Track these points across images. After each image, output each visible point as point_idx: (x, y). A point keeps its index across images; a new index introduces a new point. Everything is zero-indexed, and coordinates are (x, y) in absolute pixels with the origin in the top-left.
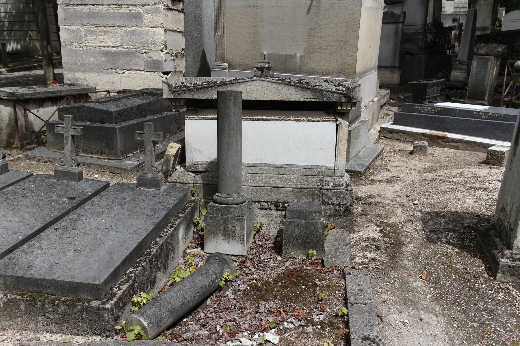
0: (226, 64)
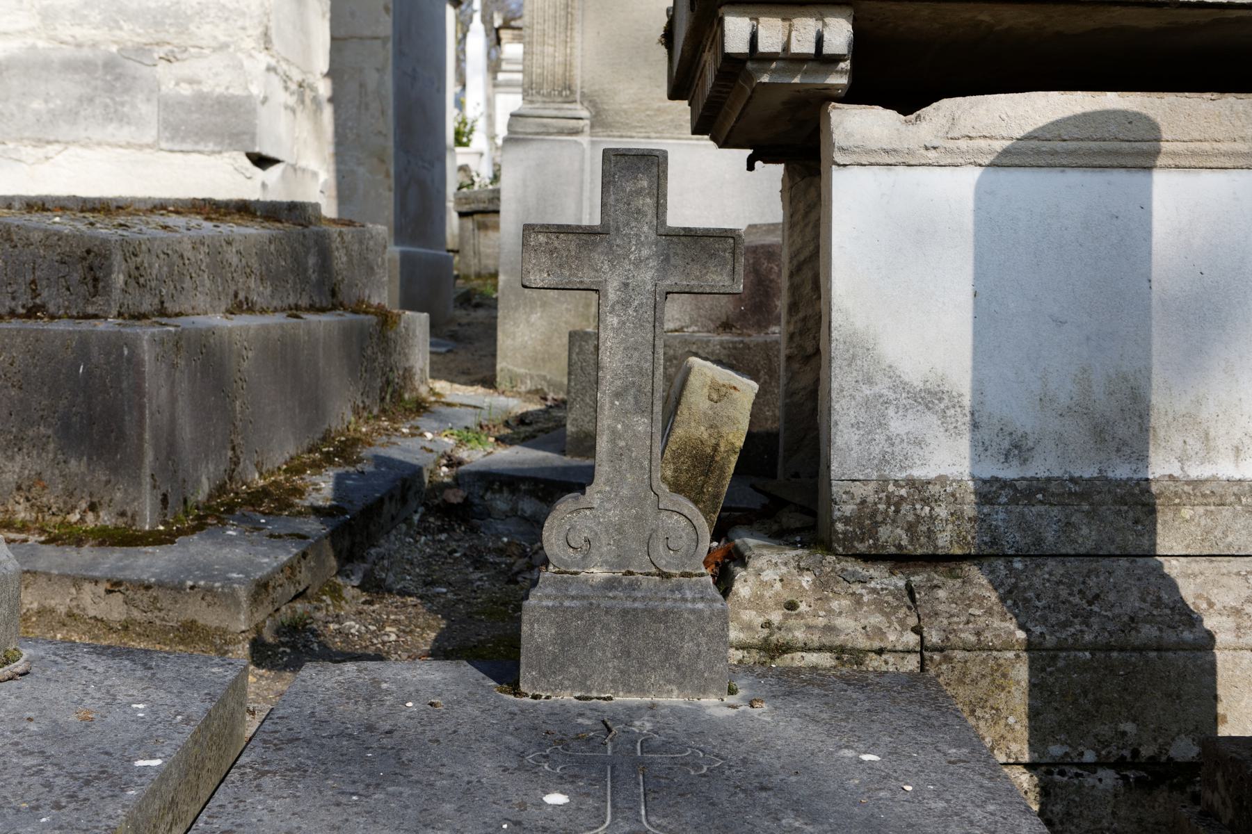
0: (585, 113)
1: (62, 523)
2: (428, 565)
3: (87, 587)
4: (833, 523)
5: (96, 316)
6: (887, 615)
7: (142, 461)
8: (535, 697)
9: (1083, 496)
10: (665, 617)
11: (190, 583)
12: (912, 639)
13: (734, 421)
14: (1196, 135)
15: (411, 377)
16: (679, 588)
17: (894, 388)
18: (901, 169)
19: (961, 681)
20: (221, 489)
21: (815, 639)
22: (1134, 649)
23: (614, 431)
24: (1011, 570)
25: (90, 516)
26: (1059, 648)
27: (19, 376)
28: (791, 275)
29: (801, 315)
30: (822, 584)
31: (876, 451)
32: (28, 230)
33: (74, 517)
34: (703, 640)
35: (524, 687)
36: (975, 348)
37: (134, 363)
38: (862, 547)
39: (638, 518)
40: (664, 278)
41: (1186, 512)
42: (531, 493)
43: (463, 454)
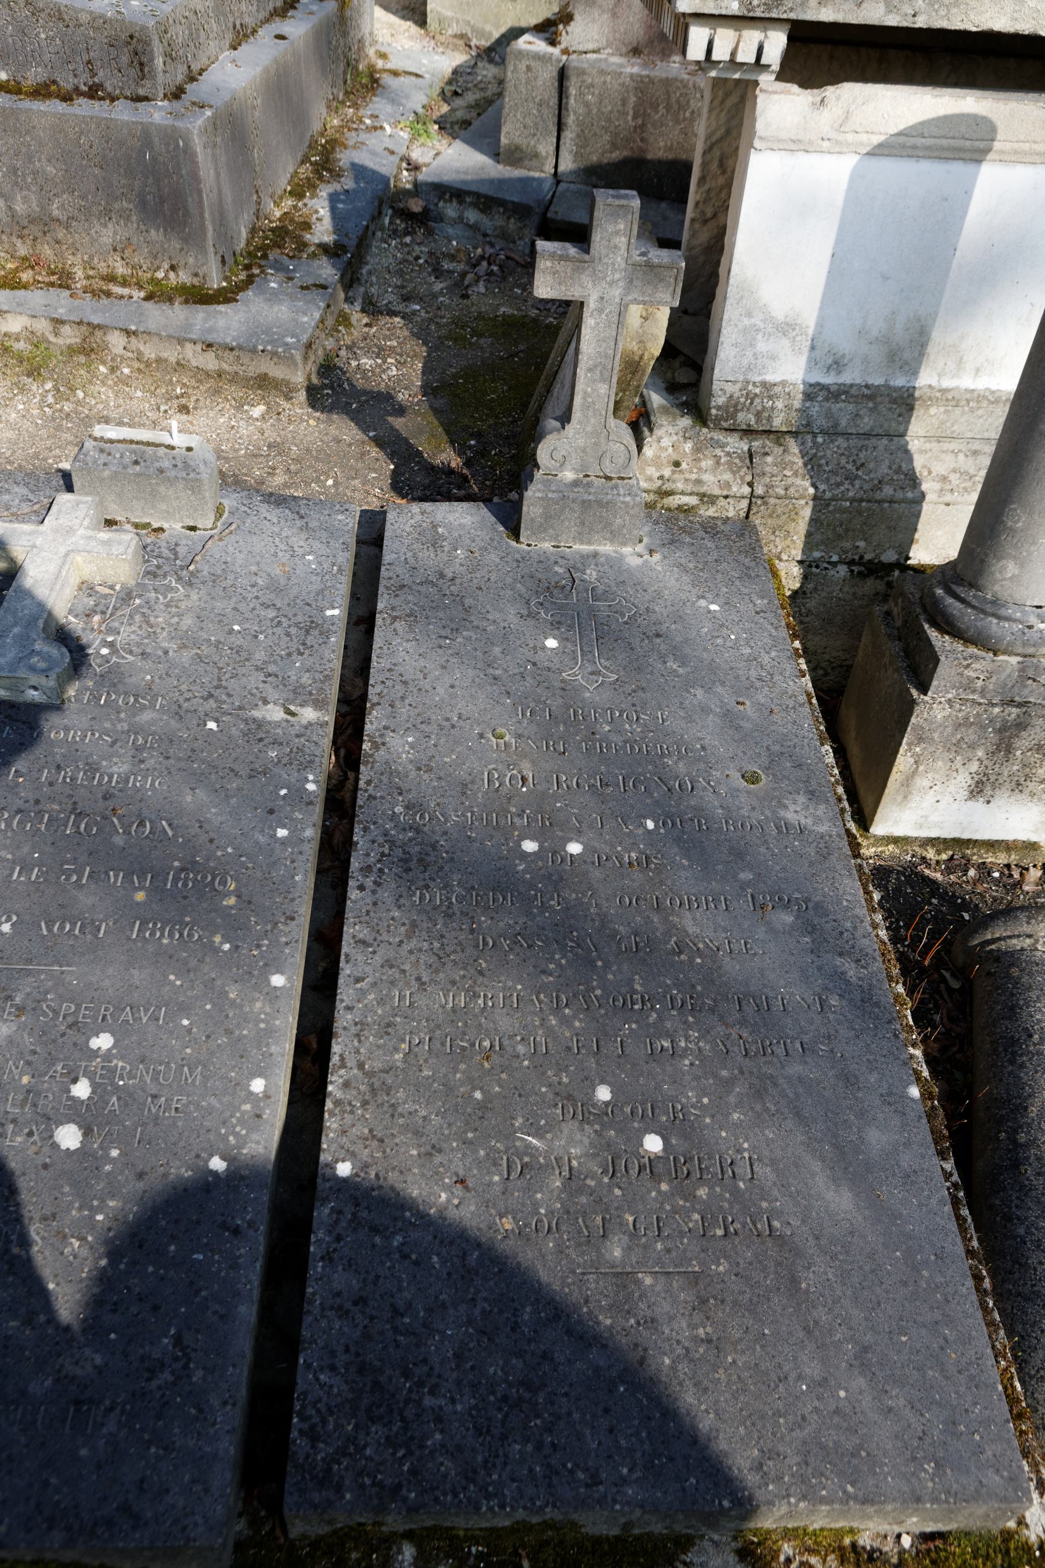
1: (152, 279)
2: (401, 273)
3: (189, 346)
4: (709, 409)
5: (146, 99)
6: (734, 473)
7: (205, 235)
8: (529, 545)
9: (871, 397)
10: (606, 505)
11: (260, 348)
12: (746, 490)
13: (655, 338)
14: (1022, 137)
15: (364, 45)
16: (616, 487)
17: (764, 321)
18: (801, 153)
19: (770, 516)
20: (253, 231)
21: (689, 488)
22: (876, 501)
23: (585, 392)
24: (814, 443)
25: (172, 275)
26: (833, 499)
27: (99, 158)
28: (704, 154)
29: (707, 187)
30: (697, 450)
31: (745, 362)
32: (76, 11)
33: (160, 275)
34: (627, 518)
35: (522, 539)
36: (824, 294)
37: (188, 152)
38: (725, 425)
39: (595, 444)
40: (628, 294)
41: (933, 411)
42: (475, 205)
43: (417, 155)
